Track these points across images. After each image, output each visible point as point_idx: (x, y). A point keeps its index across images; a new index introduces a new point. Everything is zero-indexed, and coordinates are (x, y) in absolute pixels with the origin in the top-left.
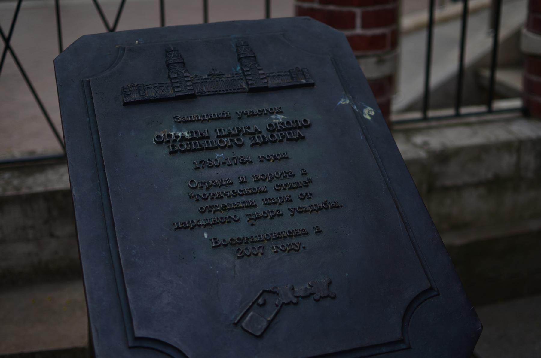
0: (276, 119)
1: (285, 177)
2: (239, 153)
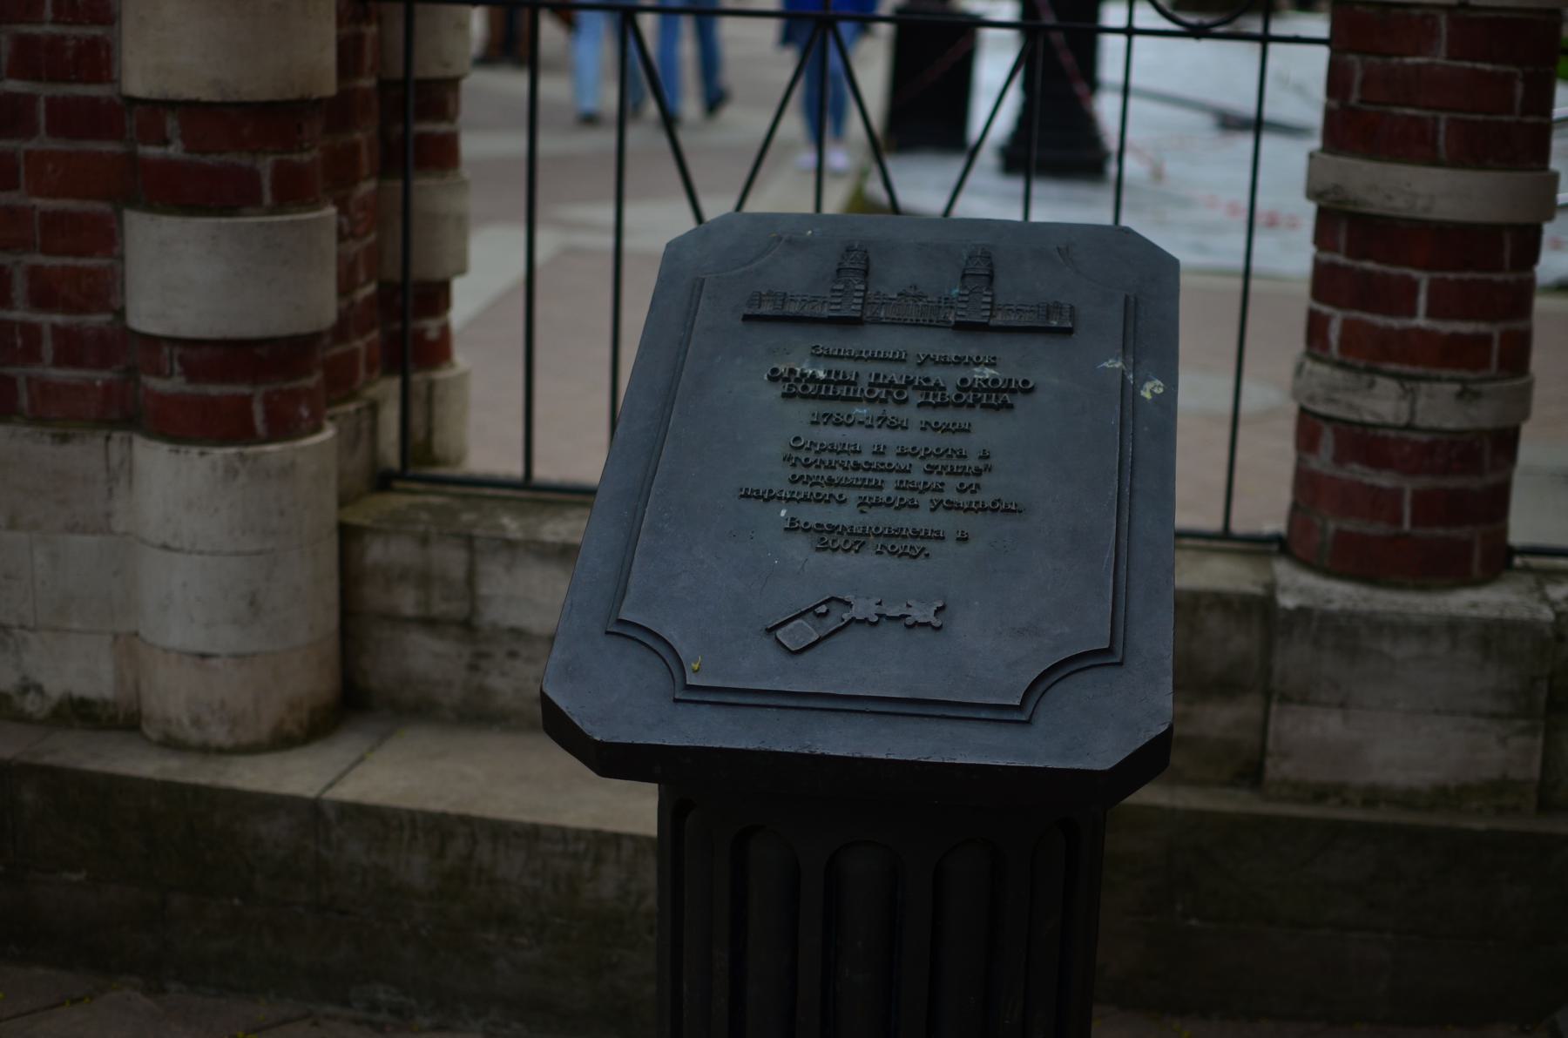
0: (980, 374)
1: (950, 456)
2: (891, 411)
